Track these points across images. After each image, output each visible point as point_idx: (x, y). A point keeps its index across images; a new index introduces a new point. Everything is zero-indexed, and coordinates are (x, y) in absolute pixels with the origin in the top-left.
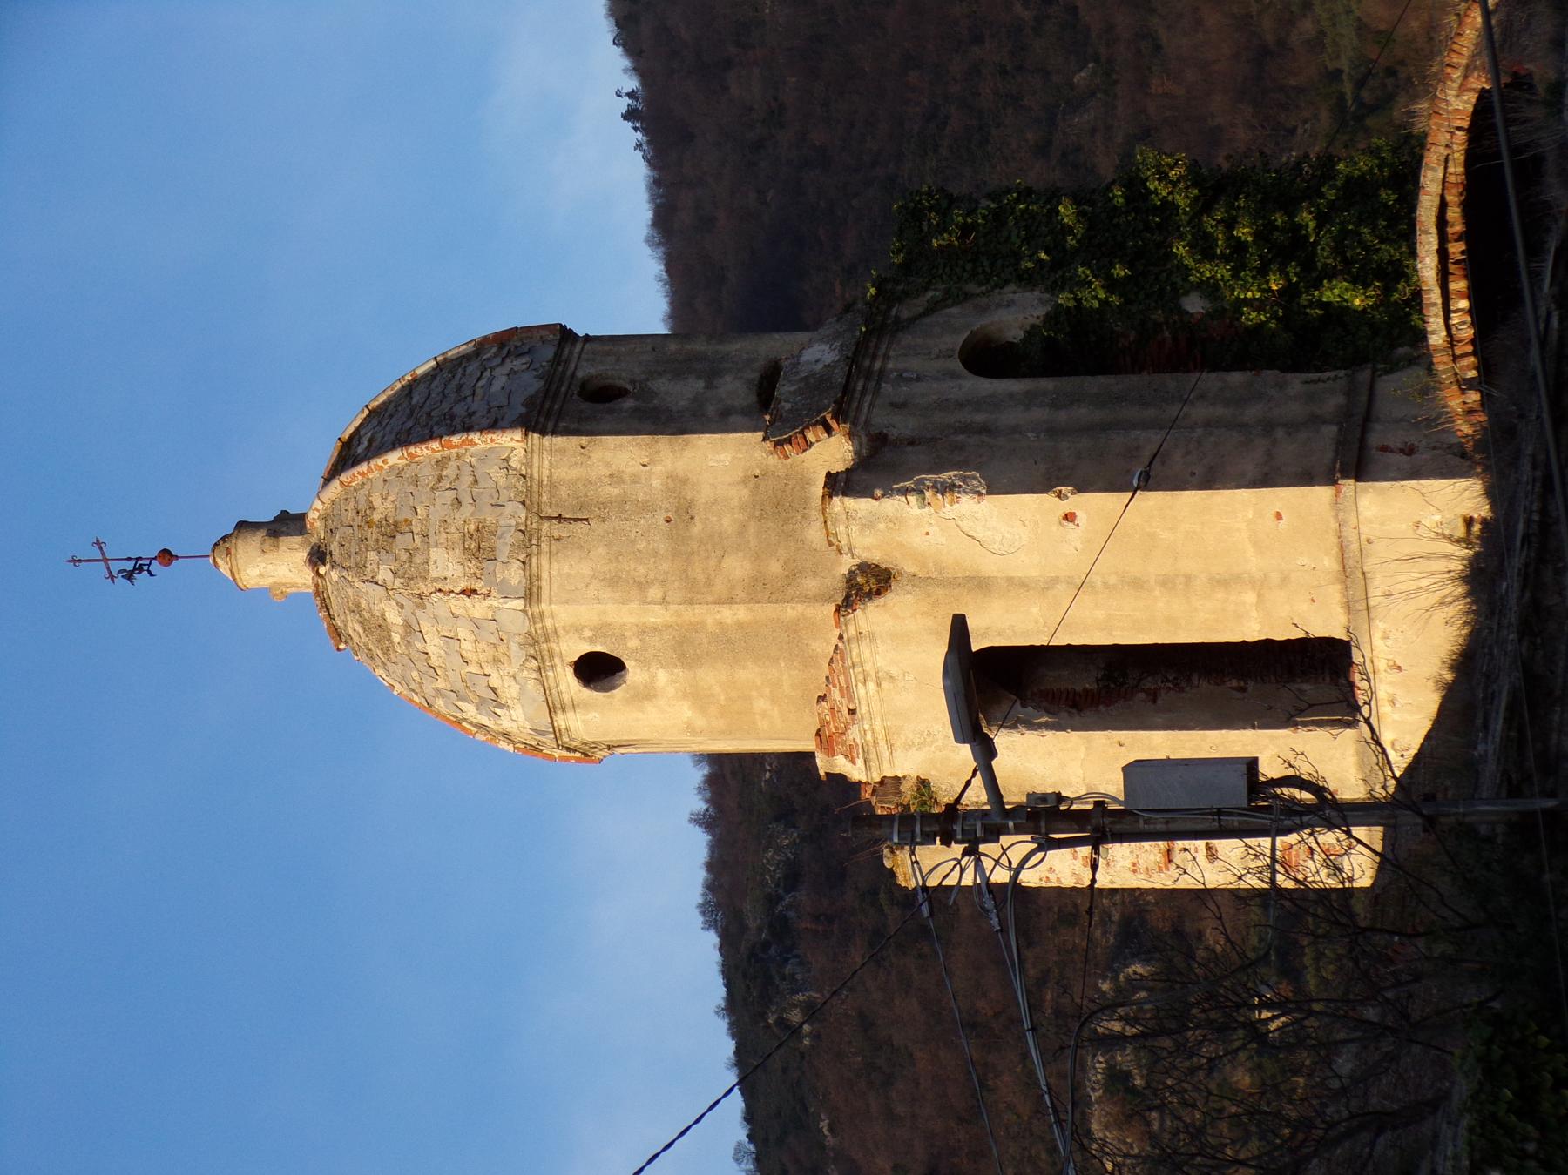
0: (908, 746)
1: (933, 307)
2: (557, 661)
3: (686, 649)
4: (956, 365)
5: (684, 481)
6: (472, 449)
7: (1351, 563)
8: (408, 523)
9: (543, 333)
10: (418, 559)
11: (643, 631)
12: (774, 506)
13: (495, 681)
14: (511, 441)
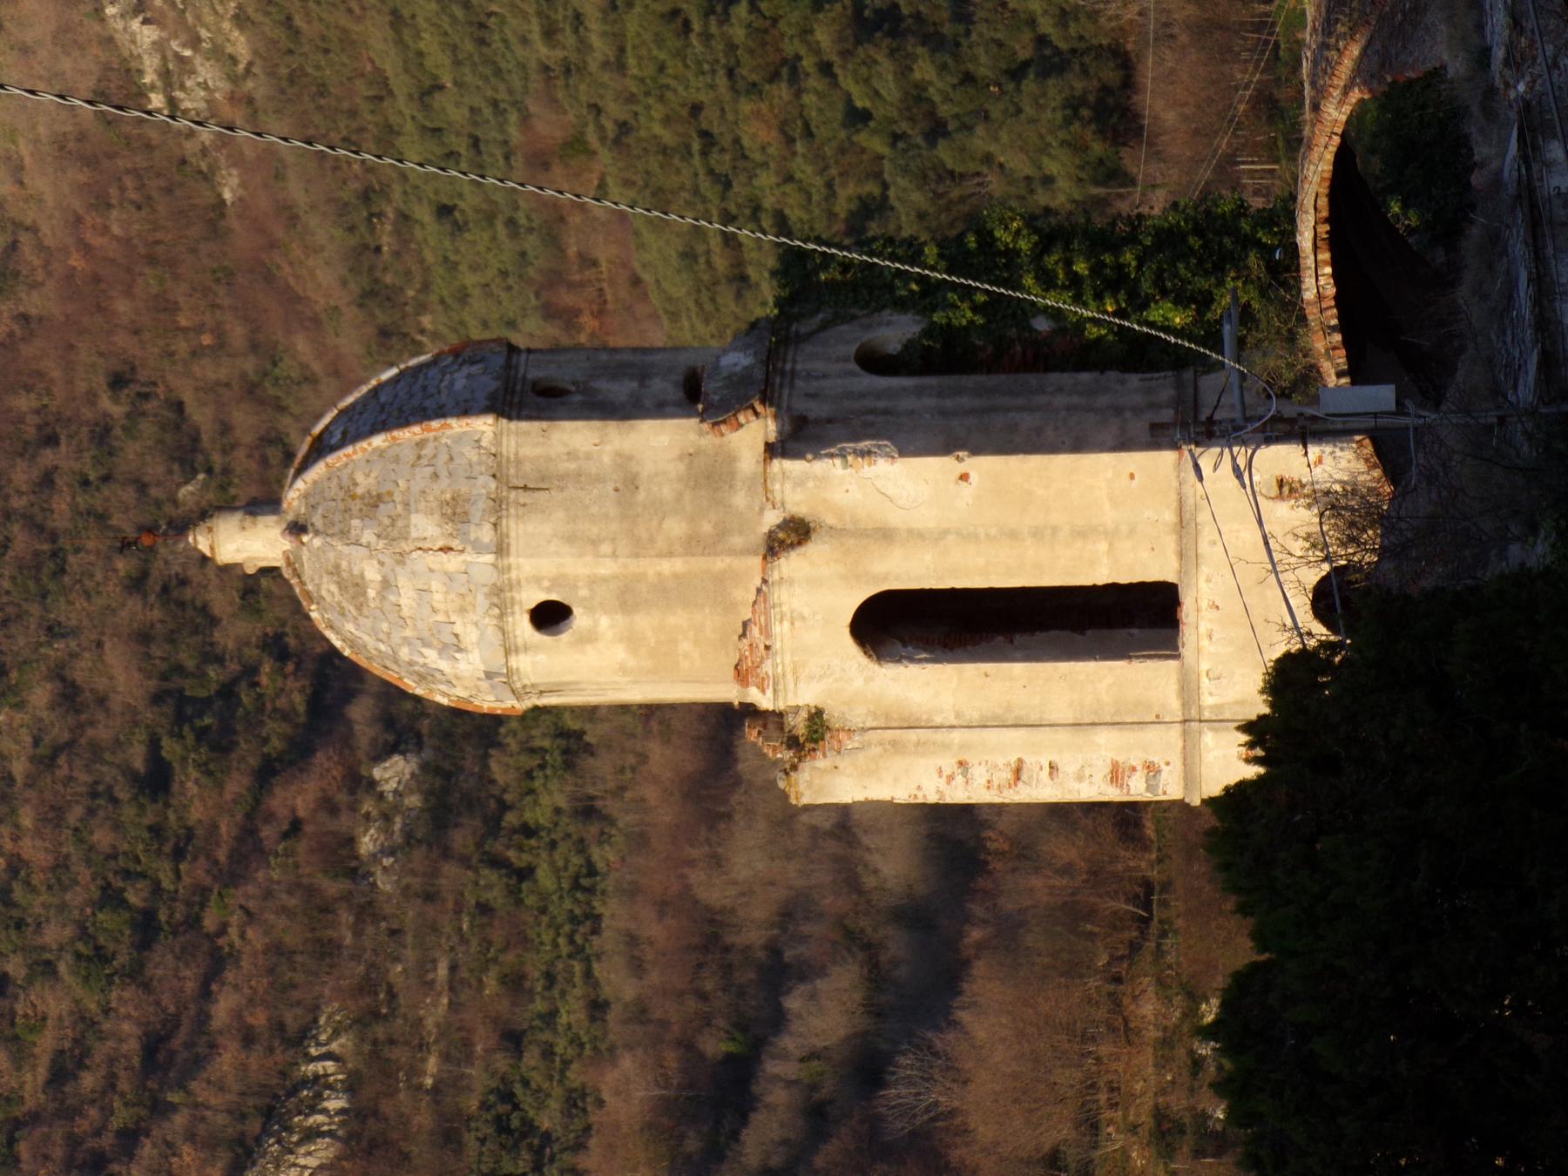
0: (811, 678)
1: (825, 326)
2: (517, 608)
3: (627, 597)
4: (856, 368)
5: (630, 458)
6: (448, 432)
7: (1187, 516)
8: (390, 494)
9: (492, 345)
10: (400, 523)
11: (593, 581)
12: (710, 478)
13: (458, 629)
14: (484, 426)
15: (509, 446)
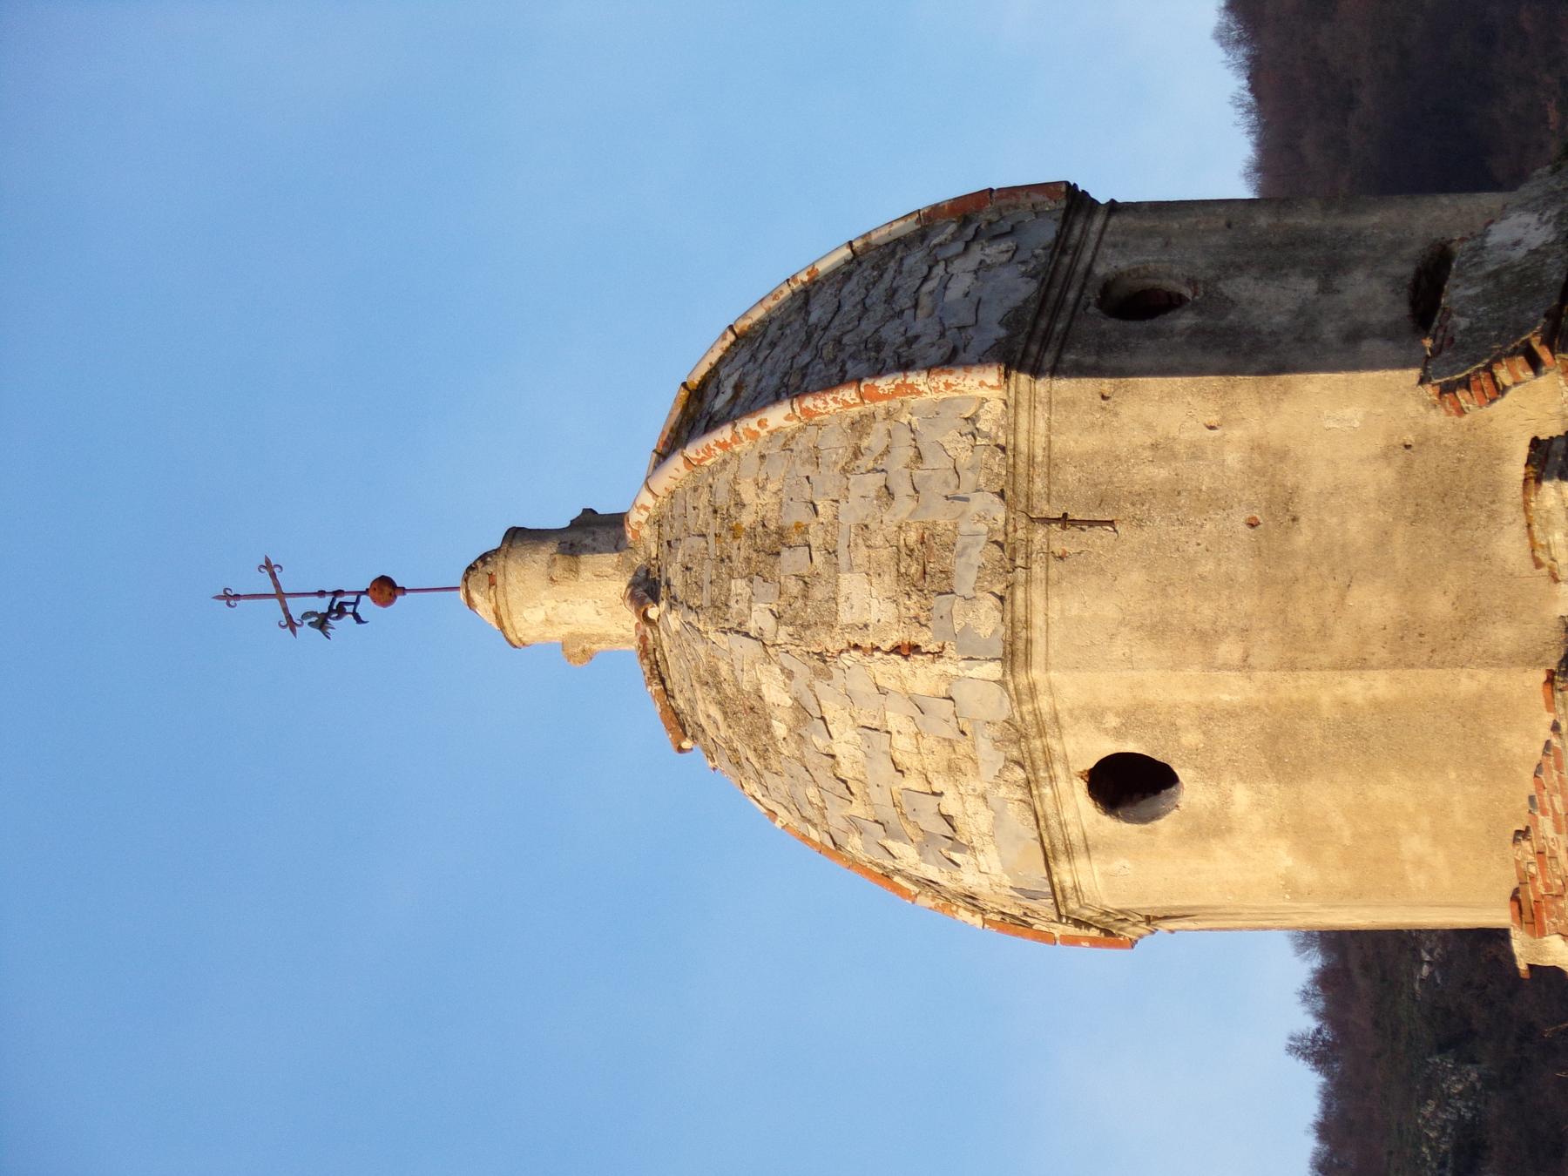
2: (1058, 769)
3: (1282, 749)
5: (1282, 455)
6: (914, 401)
8: (802, 529)
9: (1038, 198)
10: (818, 593)
11: (1208, 717)
13: (950, 805)
14: (980, 386)
15: (1034, 432)
